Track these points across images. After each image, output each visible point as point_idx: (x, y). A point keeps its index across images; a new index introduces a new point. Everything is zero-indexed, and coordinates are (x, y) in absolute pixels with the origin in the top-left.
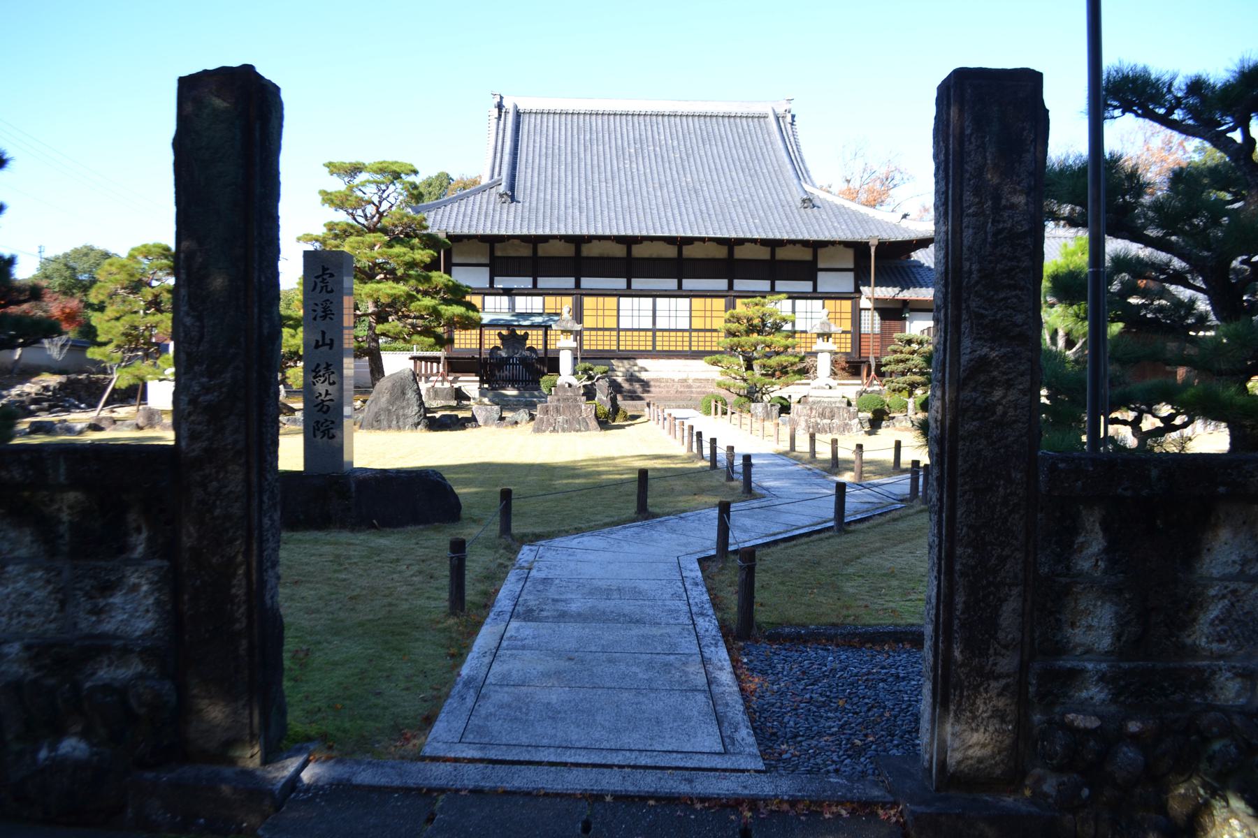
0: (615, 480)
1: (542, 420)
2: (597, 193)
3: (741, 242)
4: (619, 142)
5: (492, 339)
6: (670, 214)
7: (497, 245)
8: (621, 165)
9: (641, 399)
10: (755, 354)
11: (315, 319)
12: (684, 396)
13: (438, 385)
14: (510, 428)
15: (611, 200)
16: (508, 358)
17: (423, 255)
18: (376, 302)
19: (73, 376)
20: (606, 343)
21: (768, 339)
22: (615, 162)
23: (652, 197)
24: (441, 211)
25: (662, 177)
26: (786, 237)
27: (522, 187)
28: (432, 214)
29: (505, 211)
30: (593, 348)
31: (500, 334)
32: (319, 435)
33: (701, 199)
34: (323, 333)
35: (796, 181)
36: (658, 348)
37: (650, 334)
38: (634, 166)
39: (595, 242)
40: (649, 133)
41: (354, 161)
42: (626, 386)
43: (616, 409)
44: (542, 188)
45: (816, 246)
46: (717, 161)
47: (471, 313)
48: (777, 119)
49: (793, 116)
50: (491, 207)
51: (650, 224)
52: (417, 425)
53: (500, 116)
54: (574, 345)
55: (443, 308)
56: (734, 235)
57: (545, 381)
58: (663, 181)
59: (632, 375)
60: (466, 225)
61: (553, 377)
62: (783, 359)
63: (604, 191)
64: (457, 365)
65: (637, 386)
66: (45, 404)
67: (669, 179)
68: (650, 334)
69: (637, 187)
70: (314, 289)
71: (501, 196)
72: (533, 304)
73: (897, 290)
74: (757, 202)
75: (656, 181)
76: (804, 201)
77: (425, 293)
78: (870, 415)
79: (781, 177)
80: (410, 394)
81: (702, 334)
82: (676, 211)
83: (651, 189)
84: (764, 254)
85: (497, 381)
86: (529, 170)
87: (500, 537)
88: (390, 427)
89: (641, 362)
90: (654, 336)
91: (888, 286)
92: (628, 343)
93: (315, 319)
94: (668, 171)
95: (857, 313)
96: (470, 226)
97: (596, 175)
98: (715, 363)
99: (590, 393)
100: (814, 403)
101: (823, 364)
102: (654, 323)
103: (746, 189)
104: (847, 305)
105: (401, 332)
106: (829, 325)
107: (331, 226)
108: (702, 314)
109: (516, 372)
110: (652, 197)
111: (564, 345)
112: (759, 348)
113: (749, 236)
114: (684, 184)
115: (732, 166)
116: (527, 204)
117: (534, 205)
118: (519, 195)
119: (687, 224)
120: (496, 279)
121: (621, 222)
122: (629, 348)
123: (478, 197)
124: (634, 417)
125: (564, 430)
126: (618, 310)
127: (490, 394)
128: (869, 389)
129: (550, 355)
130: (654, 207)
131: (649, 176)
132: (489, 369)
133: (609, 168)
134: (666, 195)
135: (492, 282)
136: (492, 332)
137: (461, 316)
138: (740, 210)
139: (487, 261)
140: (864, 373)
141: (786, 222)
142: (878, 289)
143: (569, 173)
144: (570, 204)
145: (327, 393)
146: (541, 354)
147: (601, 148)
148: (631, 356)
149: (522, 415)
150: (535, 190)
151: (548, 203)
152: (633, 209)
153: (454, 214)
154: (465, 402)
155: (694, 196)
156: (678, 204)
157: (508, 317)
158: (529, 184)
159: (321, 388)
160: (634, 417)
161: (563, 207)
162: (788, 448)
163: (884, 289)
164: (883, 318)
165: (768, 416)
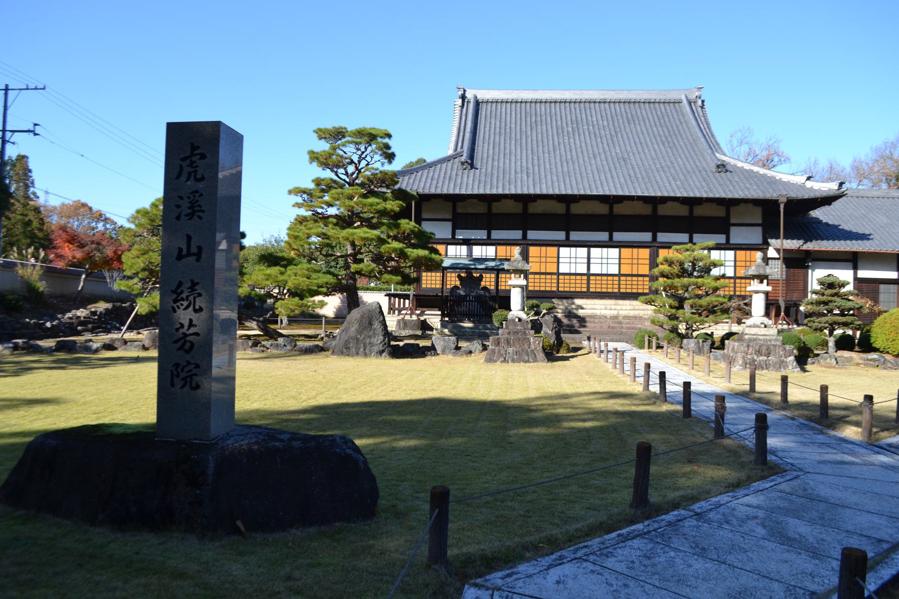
0: (580, 430)
1: (493, 350)
2: (542, 162)
3: (664, 200)
5: (453, 280)
6: (603, 178)
7: (459, 204)
8: (561, 140)
9: (578, 332)
10: (686, 295)
11: (178, 218)
12: (617, 329)
13: (407, 317)
14: (465, 358)
15: (553, 167)
16: (465, 296)
17: (393, 205)
18: (353, 244)
19: (118, 304)
20: (548, 284)
22: (556, 138)
23: (588, 165)
24: (413, 176)
25: (595, 149)
26: (705, 195)
27: (479, 157)
28: (406, 178)
29: (465, 176)
30: (537, 289)
31: (459, 276)
32: (178, 383)
34: (189, 238)
35: (709, 151)
36: (591, 290)
37: (585, 277)
38: (572, 140)
39: (540, 202)
40: (584, 116)
41: (337, 125)
42: (565, 321)
43: (560, 342)
44: (496, 158)
45: (729, 204)
46: (641, 136)
47: (433, 256)
48: (690, 103)
49: (703, 101)
50: (454, 173)
51: (587, 185)
52: (381, 353)
53: (463, 105)
54: (524, 282)
55: (409, 251)
56: (659, 194)
57: (497, 315)
58: (596, 152)
59: (570, 312)
60: (433, 186)
61: (504, 312)
62: (712, 299)
63: (547, 160)
64: (424, 301)
65: (575, 321)
66: (90, 326)
67: (601, 150)
68: (585, 277)
69: (575, 157)
70: (178, 177)
71: (463, 163)
72: (490, 251)
73: (801, 242)
74: (677, 168)
75: (591, 152)
76: (718, 166)
77: (395, 238)
79: (695, 148)
80: (377, 325)
81: (629, 278)
82: (609, 176)
83: (586, 159)
84: (683, 211)
85: (455, 315)
86: (486, 145)
87: (428, 567)
88: (357, 354)
89: (578, 302)
90: (588, 280)
91: (793, 239)
92: (565, 286)
93: (178, 218)
94: (600, 145)
96: (436, 187)
99: (537, 327)
100: (750, 340)
101: (758, 304)
102: (589, 269)
103: (666, 158)
105: (373, 270)
107: (318, 182)
108: (630, 261)
109: (473, 310)
110: (588, 165)
111: (515, 285)
113: (672, 195)
114: (614, 154)
115: (654, 140)
116: (483, 170)
117: (489, 170)
118: (478, 163)
119: (618, 186)
120: (457, 231)
121: (562, 183)
123: (444, 165)
124: (576, 349)
125: (513, 361)
126: (558, 258)
127: (450, 326)
129: (502, 295)
130: (589, 172)
131: (584, 148)
132: (447, 304)
133: (551, 142)
134: (599, 163)
135: (454, 234)
136: (453, 275)
137: (425, 257)
138: (663, 175)
139: (449, 216)
140: (773, 314)
141: (704, 184)
142: (785, 241)
143: (518, 147)
145: (191, 324)
146: (494, 293)
147: (544, 127)
148: (570, 296)
149: (476, 345)
150: (490, 159)
151: (501, 169)
152: (572, 173)
153: (424, 178)
154: (429, 332)
155: (623, 163)
156: (610, 170)
157: (466, 262)
158: (485, 155)
159: (184, 316)
160: (576, 349)
161: (513, 173)
162: (747, 388)
163: (789, 241)
165: (699, 351)
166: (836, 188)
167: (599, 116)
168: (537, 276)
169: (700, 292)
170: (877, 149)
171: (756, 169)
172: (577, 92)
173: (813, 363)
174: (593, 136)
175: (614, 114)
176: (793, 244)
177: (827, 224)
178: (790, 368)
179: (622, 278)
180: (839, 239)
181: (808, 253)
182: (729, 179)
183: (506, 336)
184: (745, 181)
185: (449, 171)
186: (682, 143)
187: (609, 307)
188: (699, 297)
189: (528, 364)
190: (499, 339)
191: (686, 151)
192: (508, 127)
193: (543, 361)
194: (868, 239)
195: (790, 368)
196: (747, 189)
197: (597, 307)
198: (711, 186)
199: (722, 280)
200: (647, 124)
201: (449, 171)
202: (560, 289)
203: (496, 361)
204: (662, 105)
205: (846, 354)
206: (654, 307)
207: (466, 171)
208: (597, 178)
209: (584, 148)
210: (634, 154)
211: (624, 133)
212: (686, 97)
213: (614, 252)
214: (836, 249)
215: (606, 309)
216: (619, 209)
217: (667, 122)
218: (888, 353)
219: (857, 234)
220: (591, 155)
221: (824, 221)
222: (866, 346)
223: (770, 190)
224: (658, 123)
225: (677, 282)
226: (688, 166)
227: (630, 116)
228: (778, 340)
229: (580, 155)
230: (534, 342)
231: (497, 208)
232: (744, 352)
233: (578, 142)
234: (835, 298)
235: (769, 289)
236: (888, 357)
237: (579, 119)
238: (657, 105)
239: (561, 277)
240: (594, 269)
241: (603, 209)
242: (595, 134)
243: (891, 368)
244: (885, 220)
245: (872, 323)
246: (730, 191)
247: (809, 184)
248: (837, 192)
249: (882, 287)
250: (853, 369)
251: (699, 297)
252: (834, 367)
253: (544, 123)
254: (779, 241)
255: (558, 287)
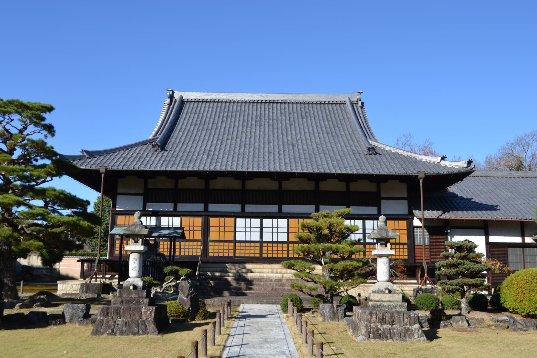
1: (101, 322)
4: (246, 118)
8: (244, 131)
21: (335, 246)
30: (216, 255)
33: (296, 150)
35: (364, 138)
36: (264, 255)
37: (258, 245)
38: (253, 130)
40: (267, 113)
42: (234, 284)
46: (310, 128)
48: (352, 104)
49: (363, 103)
58: (271, 139)
63: (228, 145)
67: (276, 138)
68: (258, 245)
72: (176, 221)
73: (440, 212)
74: (336, 151)
76: (369, 149)
78: (428, 313)
79: (353, 137)
83: (262, 144)
86: (181, 133)
89: (249, 266)
90: (261, 247)
91: (433, 210)
94: (276, 134)
95: (411, 229)
97: (226, 136)
98: (289, 267)
100: (374, 307)
101: (382, 269)
103: (328, 144)
104: (403, 224)
106: (387, 231)
112: (328, 254)
115: (320, 131)
118: (169, 147)
120: (148, 204)
122: (242, 255)
125: (122, 333)
128: (424, 287)
131: (262, 136)
139: (142, 192)
140: (419, 275)
141: (356, 163)
142: (426, 212)
144: (202, 152)
147: (233, 121)
150: (181, 144)
155: (291, 147)
156: (279, 152)
163: (430, 212)
166: (466, 165)
167: (279, 114)
168: (216, 244)
169: (336, 256)
170: (503, 148)
172: (263, 95)
173: (446, 326)
174: (271, 128)
175: (291, 112)
177: (462, 198)
178: (416, 336)
179: (290, 245)
180: (472, 210)
181: (446, 221)
183: (118, 305)
184: (391, 161)
185: (142, 152)
186: (343, 133)
187: (275, 271)
188: (335, 261)
189: (137, 337)
190: (108, 309)
191: (345, 139)
192: (203, 120)
193: (153, 333)
194: (496, 210)
195: (416, 336)
196: (392, 167)
197: (265, 270)
199: (357, 246)
200: (317, 119)
201: (142, 152)
202: (237, 255)
203: (102, 334)
204: (330, 106)
205: (478, 315)
206: (293, 271)
207: (156, 153)
208: (267, 158)
209: (262, 136)
210: (302, 141)
211: (297, 125)
212: (350, 99)
213: (283, 222)
214: (469, 218)
215: (272, 272)
216: (287, 185)
217: (333, 118)
218: (517, 313)
219: (487, 205)
220: (266, 142)
221: (460, 195)
222: (496, 306)
223: (412, 168)
224: (325, 119)
225: (313, 246)
226: (345, 150)
227: (304, 113)
228: (402, 306)
229: (257, 141)
230: (146, 312)
231: (183, 184)
232: (368, 320)
233: (258, 132)
234: (466, 262)
235: (393, 252)
236: (518, 318)
237: (263, 115)
238: (326, 105)
239: (237, 244)
240: (267, 237)
241: (273, 185)
242: (273, 126)
243: (521, 329)
244: (509, 195)
245: (501, 283)
247: (443, 163)
248: (467, 169)
249: (510, 250)
250: (484, 333)
251: (335, 261)
252: (466, 331)
253: (233, 118)
254: (421, 212)
255: (235, 253)
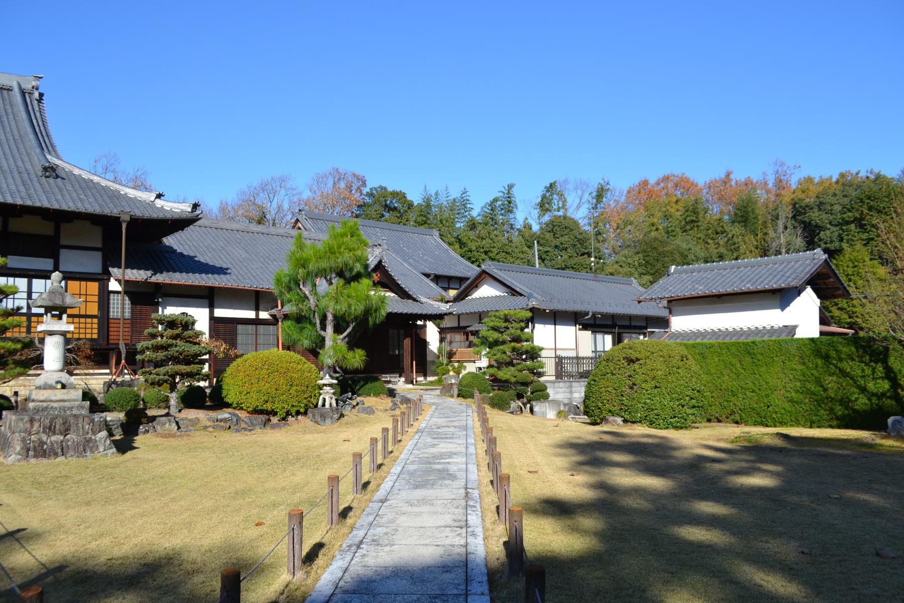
35: (38, 150)
48: (23, 93)
49: (41, 95)
73: (149, 273)
76: (45, 169)
78: (121, 416)
79: (21, 146)
95: (105, 296)
100: (37, 410)
101: (53, 354)
104: (93, 287)
128: (119, 379)
141: (22, 188)
142: (128, 271)
163: (135, 271)
164: (133, 302)
166: (190, 210)
171: (96, 179)
173: (147, 431)
176: (138, 275)
177: (181, 254)
178: (101, 449)
180: (194, 272)
181: (158, 286)
182: (58, 187)
184: (80, 192)
194: (226, 274)
195: (101, 449)
198: (32, 191)
205: (192, 414)
214: (190, 283)
218: (242, 409)
221: (179, 251)
223: (111, 205)
232: (25, 431)
235: (71, 328)
236: (242, 415)
244: (244, 255)
246: (56, 200)
247: (159, 203)
248: (190, 215)
249: (240, 327)
